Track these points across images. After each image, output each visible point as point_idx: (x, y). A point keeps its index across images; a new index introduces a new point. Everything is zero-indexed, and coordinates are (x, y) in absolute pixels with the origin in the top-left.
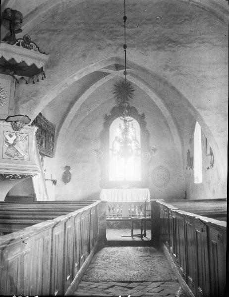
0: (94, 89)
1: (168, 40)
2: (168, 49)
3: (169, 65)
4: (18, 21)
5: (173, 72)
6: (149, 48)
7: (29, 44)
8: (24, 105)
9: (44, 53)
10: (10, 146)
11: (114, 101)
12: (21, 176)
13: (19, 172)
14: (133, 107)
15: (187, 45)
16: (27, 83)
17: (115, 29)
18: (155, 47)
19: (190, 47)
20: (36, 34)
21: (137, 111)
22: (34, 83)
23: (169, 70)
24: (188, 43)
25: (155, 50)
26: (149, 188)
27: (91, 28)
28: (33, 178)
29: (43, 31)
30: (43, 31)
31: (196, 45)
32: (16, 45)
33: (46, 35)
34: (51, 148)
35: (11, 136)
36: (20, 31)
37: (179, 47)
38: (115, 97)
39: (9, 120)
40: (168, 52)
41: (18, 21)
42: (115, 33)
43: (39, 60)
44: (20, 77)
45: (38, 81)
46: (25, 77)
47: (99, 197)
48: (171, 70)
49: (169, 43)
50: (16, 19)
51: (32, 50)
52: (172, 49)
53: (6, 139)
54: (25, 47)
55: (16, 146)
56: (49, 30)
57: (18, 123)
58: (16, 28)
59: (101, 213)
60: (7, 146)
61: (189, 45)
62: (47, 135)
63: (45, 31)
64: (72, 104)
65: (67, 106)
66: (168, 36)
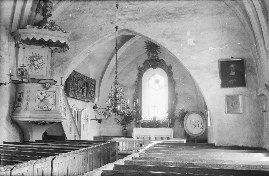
0: (126, 48)
1: (167, 13)
2: (166, 20)
3: (166, 33)
4: (48, 9)
5: (169, 40)
6: (151, 20)
7: (53, 26)
8: (57, 69)
9: (66, 32)
10: (41, 101)
11: (146, 55)
12: (49, 122)
13: (48, 119)
14: (162, 60)
15: (181, 16)
16: (59, 52)
17: (124, 7)
18: (155, 19)
19: (183, 18)
20: (66, 14)
21: (165, 63)
22: (64, 52)
23: (166, 37)
24: (182, 14)
25: (155, 22)
26: (174, 130)
27: (106, 7)
28: (62, 122)
29: (71, 12)
30: (71, 12)
31: (188, 15)
32: (44, 28)
33: (73, 15)
34: (93, 96)
35: (41, 94)
36: (50, 15)
37: (175, 18)
38: (147, 52)
39: (39, 82)
40: (166, 23)
41: (48, 9)
42: (125, 10)
43: (62, 37)
44: (54, 48)
45: (66, 51)
46: (57, 48)
47: (132, 134)
48: (168, 37)
49: (166, 15)
50: (47, 7)
51: (56, 31)
52: (169, 20)
53: (38, 96)
54: (50, 29)
55: (45, 101)
56: (75, 11)
57: (47, 84)
58: (47, 14)
59: (113, 151)
60: (39, 101)
61: (183, 16)
62: (89, 85)
63: (73, 12)
64: (110, 59)
65: (105, 62)
66: (166, 9)
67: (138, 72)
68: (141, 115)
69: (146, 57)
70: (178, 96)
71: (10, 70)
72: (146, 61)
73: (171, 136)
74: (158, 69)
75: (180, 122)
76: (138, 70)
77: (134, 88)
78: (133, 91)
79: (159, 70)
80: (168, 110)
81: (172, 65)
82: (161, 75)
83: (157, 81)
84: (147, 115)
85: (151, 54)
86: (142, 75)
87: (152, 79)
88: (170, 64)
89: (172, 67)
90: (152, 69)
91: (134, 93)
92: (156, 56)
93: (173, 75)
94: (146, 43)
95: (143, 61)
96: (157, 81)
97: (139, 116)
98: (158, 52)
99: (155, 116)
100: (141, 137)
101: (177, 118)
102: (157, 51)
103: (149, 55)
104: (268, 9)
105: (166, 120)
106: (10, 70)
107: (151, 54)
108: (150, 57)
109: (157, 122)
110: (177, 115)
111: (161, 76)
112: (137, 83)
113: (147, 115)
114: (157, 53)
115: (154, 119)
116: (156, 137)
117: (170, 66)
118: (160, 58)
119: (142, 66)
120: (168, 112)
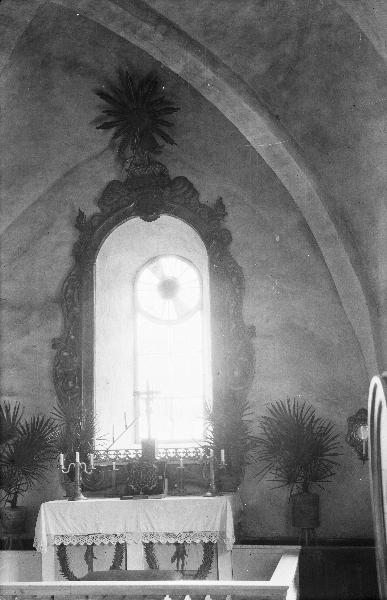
38: (112, 146)
67: (76, 239)
68: (89, 433)
69: (108, 172)
70: (257, 342)
71: (223, 451)
72: (111, 187)
73: (223, 534)
74: (164, 218)
75: (114, 77)
76: (76, 226)
77: (60, 314)
78: (56, 327)
79: (170, 226)
80: (210, 404)
81: (227, 202)
82: (185, 259)
83: (168, 287)
84: (116, 434)
85: (129, 152)
86: (96, 249)
87: (149, 279)
88: (215, 197)
89: (229, 210)
90: (136, 222)
91: (57, 335)
92: (152, 163)
93: (232, 247)
94: (101, 94)
95: (95, 191)
96: (168, 287)
97: (80, 439)
98: (160, 141)
99: (153, 437)
100: (78, 545)
101: (256, 441)
102: (155, 135)
103: (121, 158)
104: (383, 299)
105: (202, 453)
106: (223, 451)
107: (129, 152)
108: (127, 166)
109: (161, 464)
110: (256, 430)
111: (185, 265)
112: (69, 291)
113: (116, 434)
114: (157, 146)
115: (148, 449)
116: (151, 543)
117: (220, 203)
118: (174, 172)
119: (92, 210)
120: (212, 418)
